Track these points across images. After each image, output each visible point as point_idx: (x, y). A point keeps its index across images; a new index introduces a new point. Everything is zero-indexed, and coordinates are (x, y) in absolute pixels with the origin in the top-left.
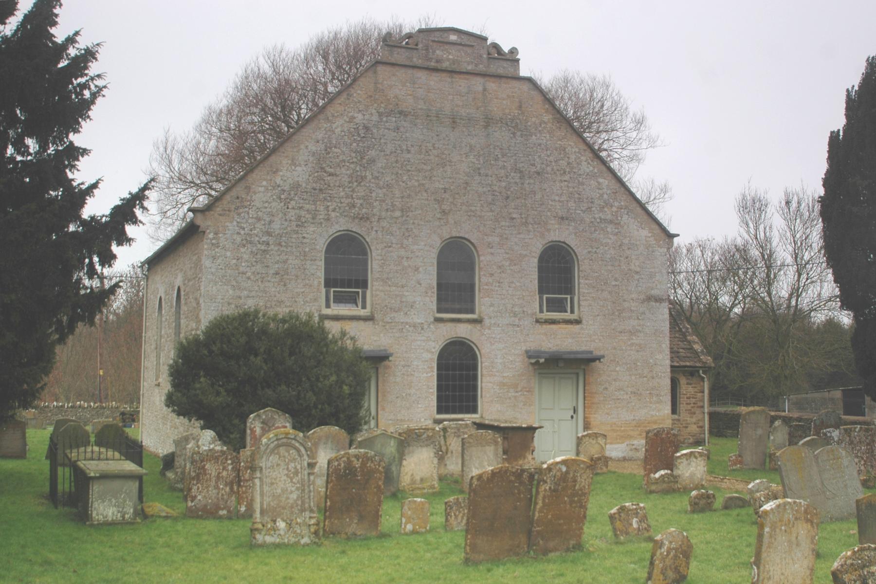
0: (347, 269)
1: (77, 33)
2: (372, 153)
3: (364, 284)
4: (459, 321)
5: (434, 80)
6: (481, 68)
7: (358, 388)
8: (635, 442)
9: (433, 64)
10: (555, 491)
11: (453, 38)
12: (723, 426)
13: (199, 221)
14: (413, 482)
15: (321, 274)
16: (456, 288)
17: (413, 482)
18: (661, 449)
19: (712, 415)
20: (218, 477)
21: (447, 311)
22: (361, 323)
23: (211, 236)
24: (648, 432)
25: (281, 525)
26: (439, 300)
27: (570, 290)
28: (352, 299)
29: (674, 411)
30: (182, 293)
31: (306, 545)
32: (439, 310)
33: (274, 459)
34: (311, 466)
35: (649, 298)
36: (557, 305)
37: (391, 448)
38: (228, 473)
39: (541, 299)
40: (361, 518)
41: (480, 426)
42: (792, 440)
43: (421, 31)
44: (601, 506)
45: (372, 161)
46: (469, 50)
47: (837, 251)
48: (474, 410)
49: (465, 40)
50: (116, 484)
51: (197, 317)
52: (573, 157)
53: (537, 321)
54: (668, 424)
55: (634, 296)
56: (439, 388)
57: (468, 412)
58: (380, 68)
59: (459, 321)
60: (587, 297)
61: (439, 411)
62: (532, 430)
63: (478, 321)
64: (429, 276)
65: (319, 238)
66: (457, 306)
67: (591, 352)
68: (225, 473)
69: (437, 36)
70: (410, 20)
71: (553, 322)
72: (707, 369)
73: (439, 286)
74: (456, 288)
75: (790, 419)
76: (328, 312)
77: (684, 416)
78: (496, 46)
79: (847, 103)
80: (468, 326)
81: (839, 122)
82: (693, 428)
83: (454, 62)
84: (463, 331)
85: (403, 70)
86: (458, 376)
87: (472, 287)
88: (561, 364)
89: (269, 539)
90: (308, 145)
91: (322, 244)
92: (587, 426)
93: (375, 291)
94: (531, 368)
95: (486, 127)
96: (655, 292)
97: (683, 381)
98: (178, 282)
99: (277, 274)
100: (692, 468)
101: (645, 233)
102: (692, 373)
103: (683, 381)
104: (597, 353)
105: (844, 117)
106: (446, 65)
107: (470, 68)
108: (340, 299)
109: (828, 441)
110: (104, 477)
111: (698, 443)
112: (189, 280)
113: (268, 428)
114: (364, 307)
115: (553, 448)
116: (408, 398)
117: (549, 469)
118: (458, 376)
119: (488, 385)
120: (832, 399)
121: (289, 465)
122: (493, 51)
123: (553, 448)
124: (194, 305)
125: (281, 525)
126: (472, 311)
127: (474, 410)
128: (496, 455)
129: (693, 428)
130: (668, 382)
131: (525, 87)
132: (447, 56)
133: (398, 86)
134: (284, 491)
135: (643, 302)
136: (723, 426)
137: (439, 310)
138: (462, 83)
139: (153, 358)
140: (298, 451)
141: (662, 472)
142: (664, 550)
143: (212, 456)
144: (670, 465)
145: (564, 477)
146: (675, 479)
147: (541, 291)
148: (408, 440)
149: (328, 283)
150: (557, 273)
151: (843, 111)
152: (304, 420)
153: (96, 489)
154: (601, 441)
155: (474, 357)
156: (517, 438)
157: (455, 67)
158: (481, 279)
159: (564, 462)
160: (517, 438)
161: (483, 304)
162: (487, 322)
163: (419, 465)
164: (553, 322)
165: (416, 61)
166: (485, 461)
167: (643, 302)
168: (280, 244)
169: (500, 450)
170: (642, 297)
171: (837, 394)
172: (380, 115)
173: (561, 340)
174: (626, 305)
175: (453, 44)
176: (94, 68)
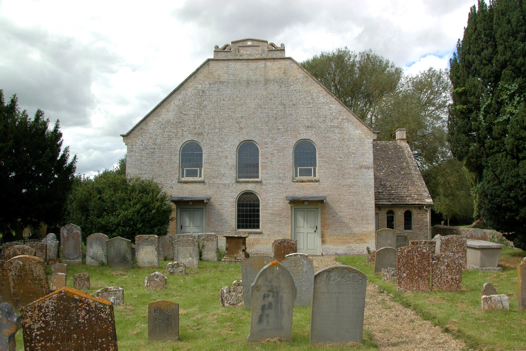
4: (248, 182)
11: (249, 43)
57: (254, 228)
59: (248, 182)
60: (321, 170)
61: (239, 227)
64: (232, 160)
66: (249, 175)
83: (249, 55)
84: (250, 187)
95: (265, 84)
96: (365, 163)
101: (358, 132)
106: (244, 57)
118: (248, 213)
132: (245, 53)
165: (230, 57)
172: (210, 84)
173: (306, 190)
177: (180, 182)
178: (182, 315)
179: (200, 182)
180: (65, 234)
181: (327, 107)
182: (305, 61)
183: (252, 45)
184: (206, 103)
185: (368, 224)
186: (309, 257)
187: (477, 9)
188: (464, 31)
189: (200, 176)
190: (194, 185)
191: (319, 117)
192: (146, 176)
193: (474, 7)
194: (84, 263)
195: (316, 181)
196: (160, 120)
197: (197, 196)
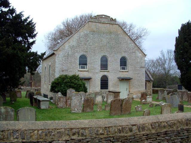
0: (83, 62)
1: (29, 16)
2: (88, 39)
3: (86, 64)
4: (105, 71)
5: (100, 25)
6: (109, 22)
7: (157, 97)
8: (138, 95)
9: (100, 22)
10: (126, 103)
11: (104, 17)
12: (155, 92)
13: (55, 52)
14: (98, 102)
15: (78, 63)
16: (104, 66)
17: (98, 102)
18: (144, 96)
19: (153, 90)
20: (63, 101)
21: (102, 70)
22: (51, 58)
23: (57, 55)
24: (141, 93)
25: (76, 109)
26: (101, 68)
27: (126, 66)
28: (84, 68)
29: (146, 89)
30: (51, 66)
31: (81, 113)
32: (101, 70)
33: (75, 97)
34: (81, 99)
35: (141, 67)
36: (124, 69)
37: (94, 96)
38: (65, 100)
39: (121, 67)
40: (90, 108)
41: (110, 92)
42: (168, 94)
43: (97, 15)
44: (133, 107)
45: (88, 41)
46: (107, 19)
47: (177, 59)
48: (107, 89)
49: (106, 17)
50: (45, 102)
51: (55, 71)
52: (127, 40)
53: (120, 72)
54: (145, 91)
55: (138, 67)
56: (101, 85)
57: (106, 89)
58: (89, 22)
59: (105, 71)
60: (129, 67)
61: (101, 89)
62: (120, 92)
63: (109, 72)
64: (99, 63)
65: (78, 56)
66: (104, 69)
67: (130, 78)
68: (64, 100)
69: (100, 16)
70: (95, 13)
71: (123, 72)
72: (152, 81)
73: (101, 65)
74: (104, 66)
75: (168, 90)
76: (79, 70)
77: (147, 90)
78: (112, 18)
79: (179, 32)
80: (107, 73)
81: (177, 35)
82: (149, 92)
83: (104, 21)
84: (106, 73)
85: (94, 23)
86: (104, 83)
87: (107, 65)
88: (124, 80)
89: (74, 112)
90: (76, 37)
91: (78, 57)
92: (129, 92)
93: (88, 66)
94: (119, 81)
95: (110, 34)
96: (142, 66)
97: (147, 83)
98: (50, 64)
99: (70, 62)
100: (149, 99)
101: (141, 54)
102: (149, 81)
103: (147, 83)
104: (131, 78)
105: (174, 42)
106: (102, 22)
107: (107, 22)
108: (82, 68)
109: (174, 94)
110: (43, 101)
111: (151, 95)
112: (53, 64)
113: (71, 92)
114: (86, 69)
115: (123, 96)
116: (94, 87)
117: (125, 99)
118: (104, 83)
119: (110, 84)
120: (176, 87)
121: (76, 99)
122: (111, 19)
123: (123, 96)
124: (54, 68)
125: (76, 109)
126: (107, 70)
127: (107, 89)
128: (113, 97)
129: (149, 92)
130: (145, 83)
131: (118, 26)
132: (103, 20)
133: (93, 26)
134: (76, 103)
135: (140, 68)
136: (155, 92)
137: (101, 70)
138: (105, 25)
139: (44, 79)
140: (79, 96)
141: (144, 100)
142: (145, 112)
143: (60, 97)
144: (145, 99)
145: (127, 101)
146: (146, 101)
147: (121, 66)
148: (96, 94)
149: (80, 64)
150: (123, 63)
151: (175, 41)
152: (77, 90)
153: (41, 103)
154: (132, 94)
155: (108, 79)
156: (117, 94)
157: (104, 22)
158: (109, 63)
159: (127, 98)
160: (117, 94)
161: (109, 68)
162: (110, 72)
163: (99, 99)
164: (123, 72)
165: (96, 21)
166: (110, 99)
167: (140, 68)
168: (70, 57)
169: (114, 96)
170: (140, 67)
171: (177, 86)
172: (90, 32)
173: (124, 75)
174: (137, 68)
175: (104, 18)
176: (35, 25)
177: (79, 71)
178: (177, 108)
179: (87, 71)
180: (69, 93)
181: (131, 45)
182: (87, 14)
183: (102, 16)
184: (88, 39)
185: (143, 87)
186: (134, 99)
187: (190, 22)
188: (181, 26)
189: (86, 69)
190: (85, 72)
191: (128, 48)
192: (65, 68)
193: (189, 21)
194: (55, 104)
195: (128, 72)
196: (70, 45)
197: (87, 77)
